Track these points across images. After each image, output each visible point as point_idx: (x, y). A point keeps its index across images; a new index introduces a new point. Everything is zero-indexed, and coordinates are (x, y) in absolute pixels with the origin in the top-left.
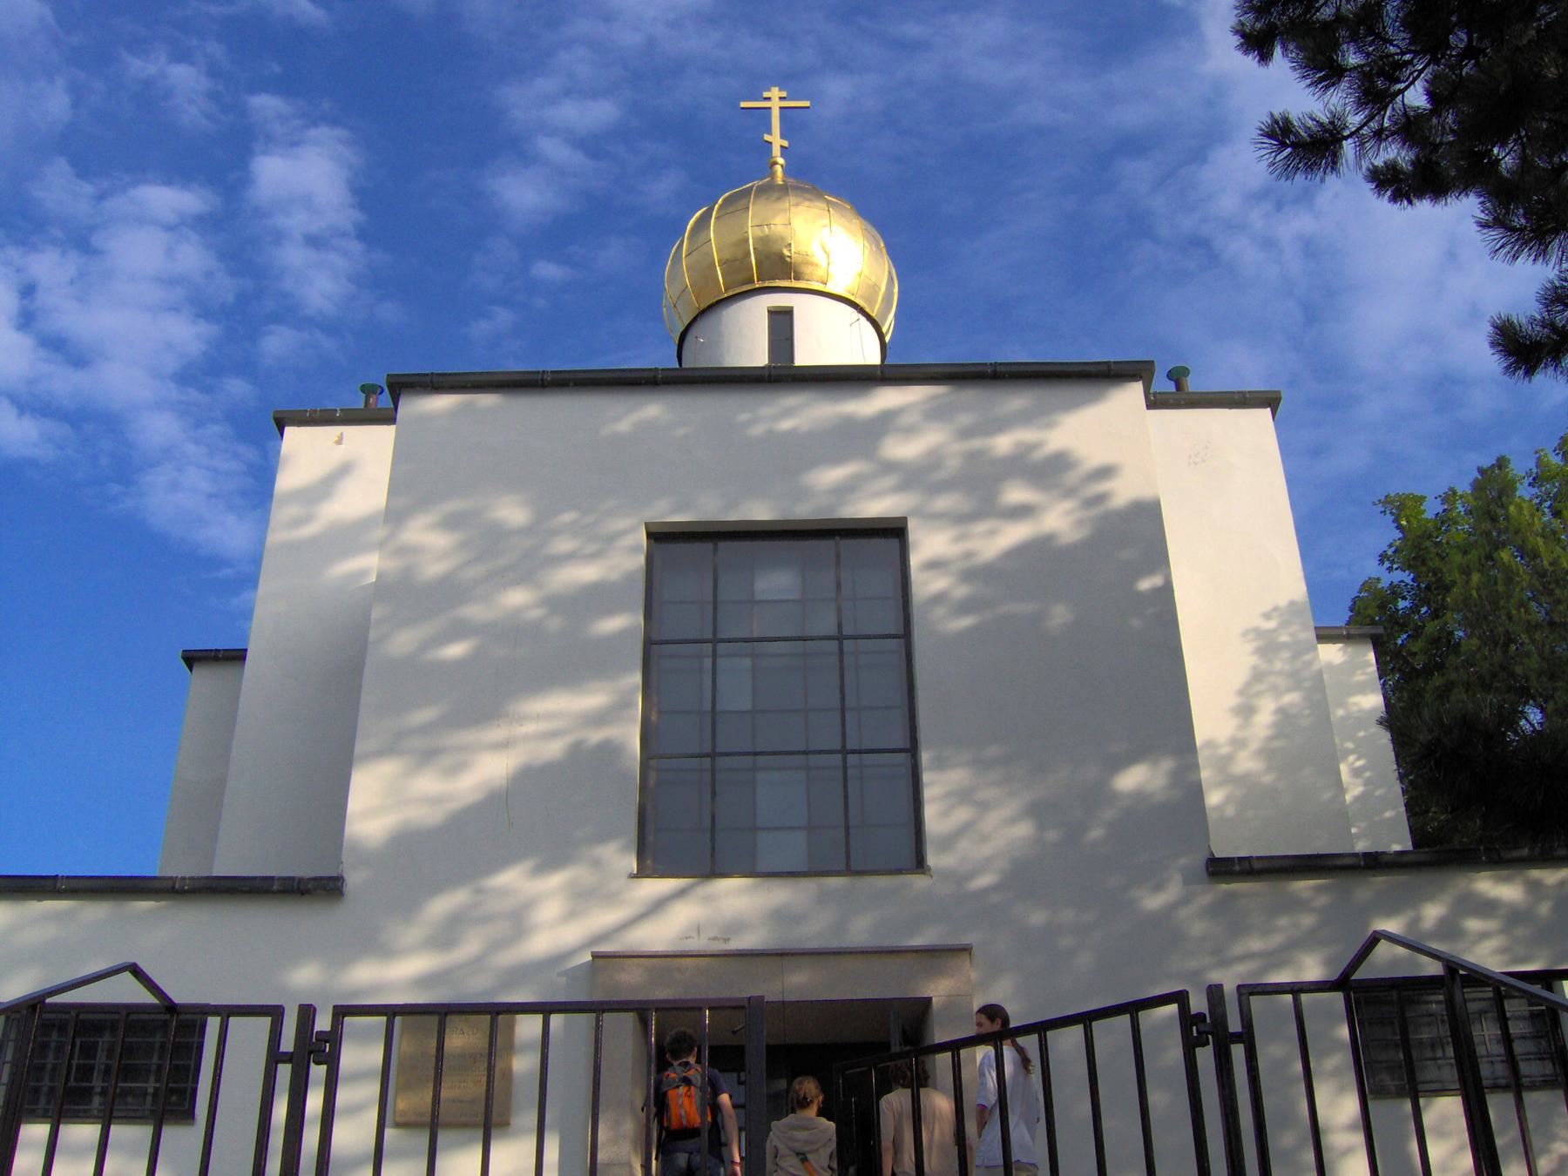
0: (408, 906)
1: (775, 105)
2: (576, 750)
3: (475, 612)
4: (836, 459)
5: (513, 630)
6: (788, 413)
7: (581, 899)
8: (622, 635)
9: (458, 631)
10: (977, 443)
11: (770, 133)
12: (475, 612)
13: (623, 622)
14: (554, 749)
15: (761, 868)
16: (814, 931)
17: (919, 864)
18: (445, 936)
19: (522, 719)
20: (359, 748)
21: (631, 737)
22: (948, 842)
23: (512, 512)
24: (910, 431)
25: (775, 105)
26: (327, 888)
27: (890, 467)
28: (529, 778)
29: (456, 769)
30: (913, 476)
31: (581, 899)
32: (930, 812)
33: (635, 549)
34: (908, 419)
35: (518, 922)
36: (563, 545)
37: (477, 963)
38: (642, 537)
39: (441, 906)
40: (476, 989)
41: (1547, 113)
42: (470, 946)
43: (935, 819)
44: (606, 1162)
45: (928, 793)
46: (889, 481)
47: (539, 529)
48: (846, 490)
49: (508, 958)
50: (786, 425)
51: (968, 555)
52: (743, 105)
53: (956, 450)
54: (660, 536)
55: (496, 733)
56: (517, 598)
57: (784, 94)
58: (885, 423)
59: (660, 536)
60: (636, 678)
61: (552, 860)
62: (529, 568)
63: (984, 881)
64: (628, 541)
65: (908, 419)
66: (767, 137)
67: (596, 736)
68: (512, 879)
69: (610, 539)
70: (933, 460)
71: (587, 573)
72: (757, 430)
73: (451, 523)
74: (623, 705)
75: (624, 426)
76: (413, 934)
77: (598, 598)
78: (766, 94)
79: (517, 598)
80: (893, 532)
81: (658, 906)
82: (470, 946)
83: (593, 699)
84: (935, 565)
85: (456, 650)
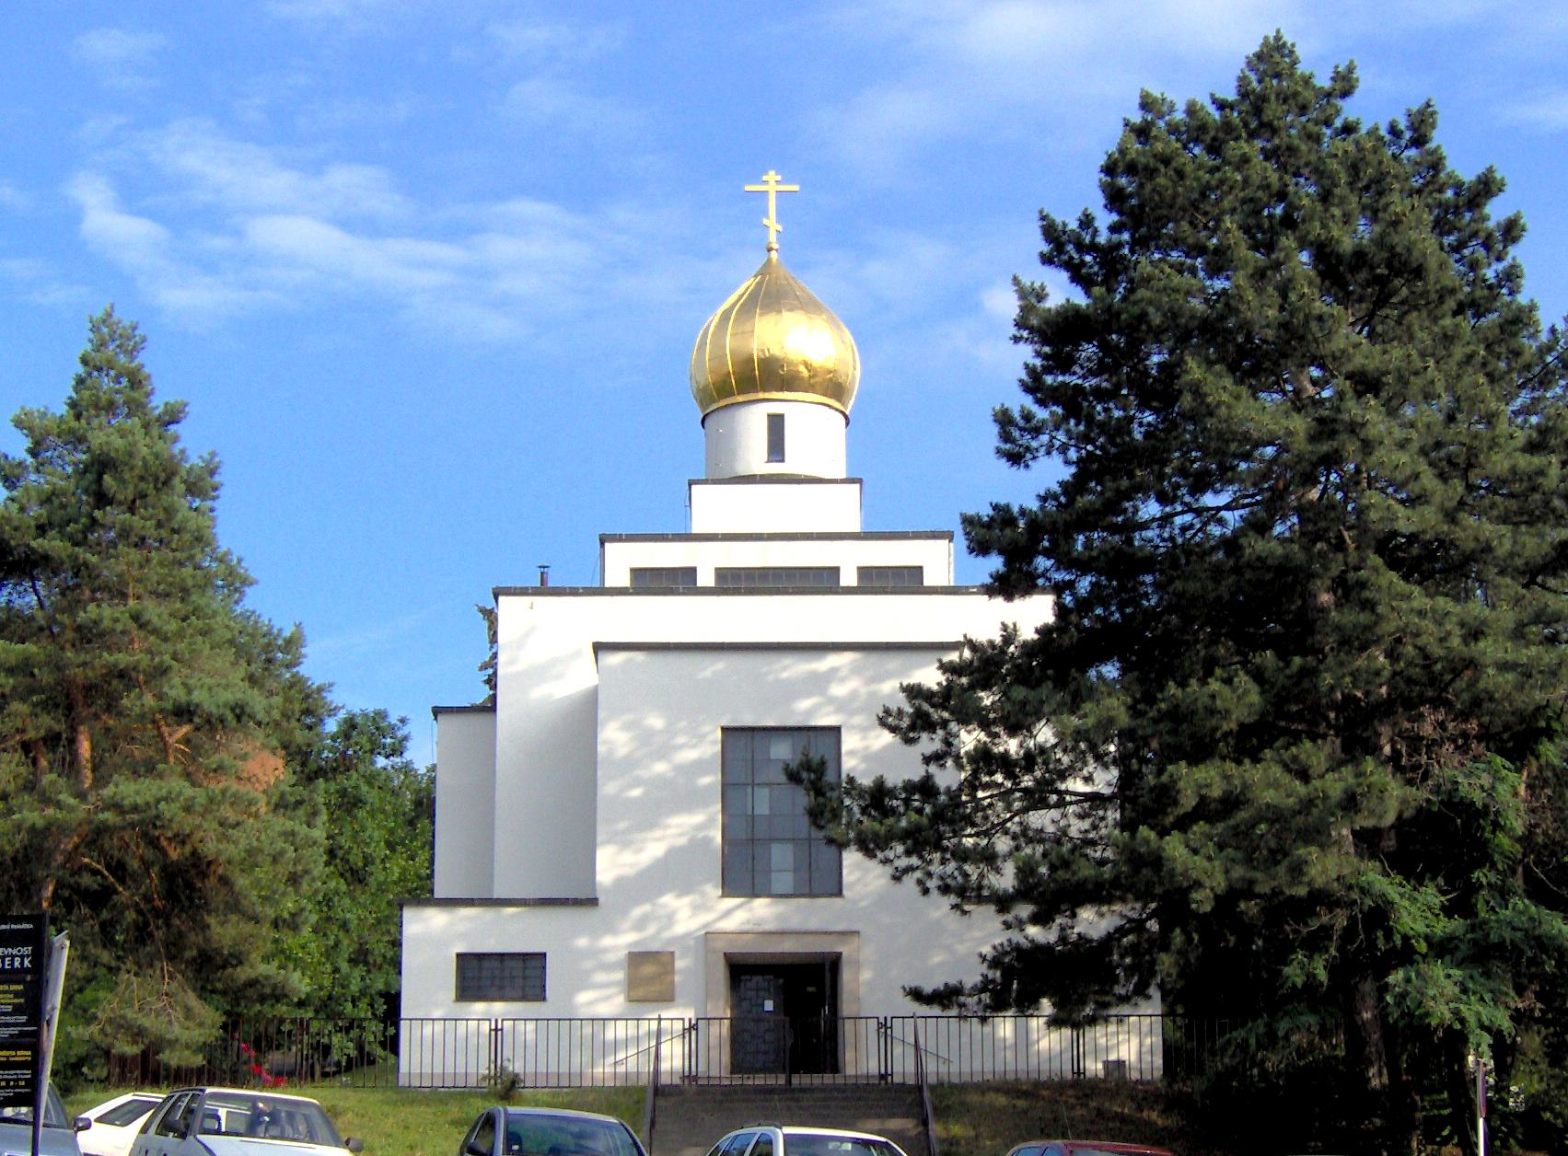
0: (624, 912)
1: (772, 188)
2: (692, 840)
3: (643, 773)
4: (809, 695)
5: (661, 783)
6: (785, 669)
7: (697, 909)
8: (708, 787)
9: (637, 783)
10: (874, 687)
11: (767, 217)
12: (643, 773)
13: (712, 779)
14: (682, 841)
15: (774, 892)
16: (795, 923)
17: (839, 893)
18: (640, 925)
19: (669, 827)
20: (599, 839)
21: (717, 836)
22: (852, 884)
23: (656, 722)
24: (842, 680)
25: (772, 188)
26: (593, 902)
27: (832, 700)
28: (672, 853)
29: (639, 851)
30: (841, 705)
31: (697, 909)
32: (845, 872)
33: (713, 743)
34: (843, 673)
35: (670, 918)
36: (681, 740)
37: (654, 937)
38: (719, 733)
39: (637, 912)
40: (654, 947)
41: (982, 694)
42: (651, 930)
43: (848, 876)
44: (769, 927)
45: (845, 863)
46: (831, 708)
47: (669, 731)
48: (810, 712)
49: (667, 935)
50: (785, 675)
51: (867, 748)
52: (748, 188)
53: (864, 690)
54: (724, 730)
55: (658, 833)
56: (660, 767)
57: (779, 178)
58: (831, 675)
59: (724, 730)
60: (719, 806)
61: (684, 891)
62: (664, 752)
63: (863, 904)
64: (711, 737)
65: (843, 673)
66: (765, 221)
67: (701, 835)
68: (668, 900)
69: (702, 737)
70: (854, 695)
71: (689, 755)
72: (771, 678)
73: (626, 727)
74: (711, 820)
75: (708, 673)
76: (626, 925)
77: (698, 767)
78: (765, 178)
79: (660, 767)
80: (836, 730)
81: (728, 913)
82: (651, 930)
83: (698, 818)
84: (852, 753)
85: (636, 792)
